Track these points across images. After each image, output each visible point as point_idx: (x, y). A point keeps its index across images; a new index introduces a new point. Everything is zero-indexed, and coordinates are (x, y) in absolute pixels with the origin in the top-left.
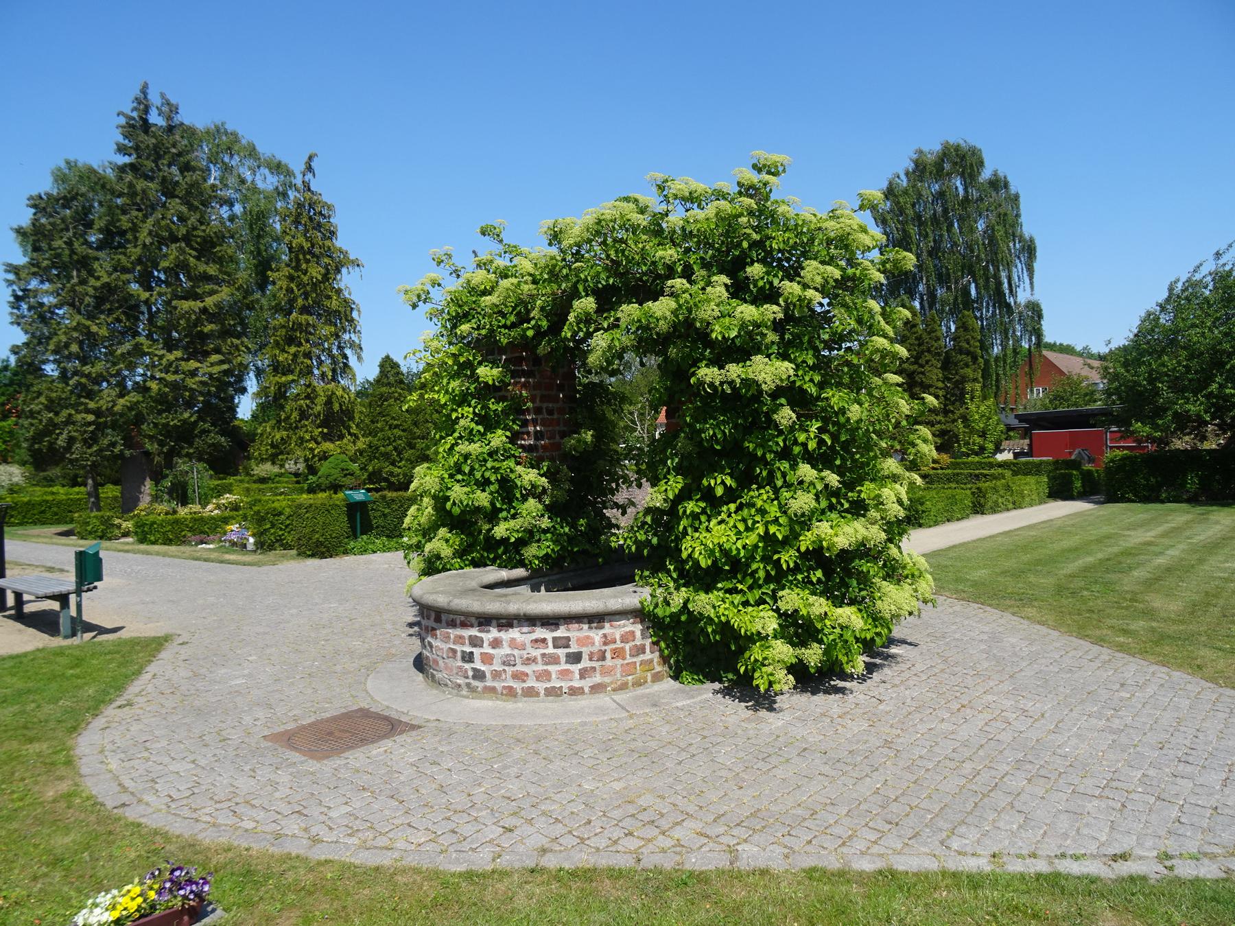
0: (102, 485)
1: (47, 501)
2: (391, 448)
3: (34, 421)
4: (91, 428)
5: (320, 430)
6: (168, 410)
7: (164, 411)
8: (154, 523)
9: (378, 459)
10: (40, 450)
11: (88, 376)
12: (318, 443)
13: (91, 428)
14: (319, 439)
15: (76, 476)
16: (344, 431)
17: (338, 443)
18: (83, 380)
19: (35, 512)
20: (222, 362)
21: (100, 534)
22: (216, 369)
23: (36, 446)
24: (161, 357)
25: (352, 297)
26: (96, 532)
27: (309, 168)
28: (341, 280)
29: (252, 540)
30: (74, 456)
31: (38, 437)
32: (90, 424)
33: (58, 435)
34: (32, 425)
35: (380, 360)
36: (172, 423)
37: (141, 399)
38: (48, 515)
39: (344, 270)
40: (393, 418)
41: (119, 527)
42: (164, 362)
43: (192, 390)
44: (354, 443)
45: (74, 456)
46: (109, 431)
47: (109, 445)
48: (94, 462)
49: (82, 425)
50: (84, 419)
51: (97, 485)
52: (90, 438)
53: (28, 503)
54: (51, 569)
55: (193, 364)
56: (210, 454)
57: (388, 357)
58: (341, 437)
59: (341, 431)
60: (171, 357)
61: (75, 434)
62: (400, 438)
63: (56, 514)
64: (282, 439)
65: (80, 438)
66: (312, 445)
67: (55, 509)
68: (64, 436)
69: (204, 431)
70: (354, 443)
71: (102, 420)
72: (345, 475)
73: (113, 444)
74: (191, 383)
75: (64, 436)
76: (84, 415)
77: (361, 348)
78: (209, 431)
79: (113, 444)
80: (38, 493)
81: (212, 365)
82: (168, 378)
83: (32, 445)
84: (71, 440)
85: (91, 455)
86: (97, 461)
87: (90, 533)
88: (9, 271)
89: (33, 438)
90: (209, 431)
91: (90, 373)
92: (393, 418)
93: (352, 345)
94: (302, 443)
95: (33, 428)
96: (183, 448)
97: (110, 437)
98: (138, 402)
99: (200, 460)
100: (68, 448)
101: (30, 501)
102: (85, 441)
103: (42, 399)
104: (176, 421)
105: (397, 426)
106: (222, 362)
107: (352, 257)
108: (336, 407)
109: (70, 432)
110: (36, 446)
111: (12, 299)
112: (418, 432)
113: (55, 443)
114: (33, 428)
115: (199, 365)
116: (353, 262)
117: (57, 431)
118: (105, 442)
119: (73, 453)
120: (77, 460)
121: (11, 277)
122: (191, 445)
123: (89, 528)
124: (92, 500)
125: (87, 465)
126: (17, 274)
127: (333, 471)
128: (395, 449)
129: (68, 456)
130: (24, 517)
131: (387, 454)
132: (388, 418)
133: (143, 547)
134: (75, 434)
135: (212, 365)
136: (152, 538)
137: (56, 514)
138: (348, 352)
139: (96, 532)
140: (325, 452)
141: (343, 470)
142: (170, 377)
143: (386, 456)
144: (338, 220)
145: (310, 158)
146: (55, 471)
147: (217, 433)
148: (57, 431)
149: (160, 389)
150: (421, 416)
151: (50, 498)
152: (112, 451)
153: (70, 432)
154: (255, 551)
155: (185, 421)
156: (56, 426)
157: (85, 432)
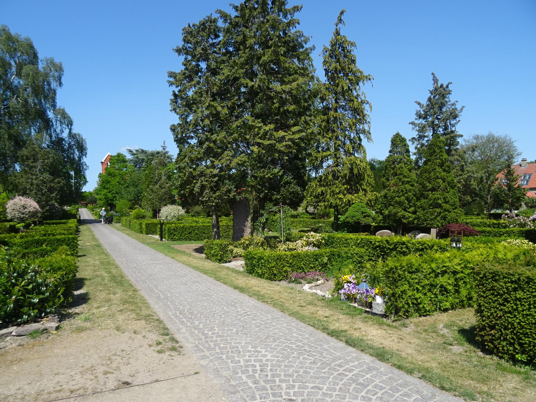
0: (220, 216)
1: (192, 227)
2: (403, 198)
3: (181, 174)
4: (216, 179)
5: (346, 186)
6: (264, 167)
7: (262, 168)
8: (261, 258)
9: (393, 206)
10: (184, 194)
11: (215, 142)
12: (345, 195)
13: (216, 179)
14: (345, 192)
15: (209, 212)
16: (359, 187)
17: (355, 195)
18: (212, 145)
19: (186, 233)
20: (300, 131)
21: (219, 258)
22: (297, 136)
23: (182, 192)
24: (260, 128)
25: (366, 99)
26: (217, 255)
27: (340, 20)
28: (359, 89)
29: (379, 300)
30: (204, 199)
31: (182, 186)
32: (215, 176)
33: (195, 184)
34: (180, 177)
35: (392, 136)
36: (267, 176)
37: (247, 160)
38: (193, 235)
39: (361, 84)
40: (405, 176)
41: (232, 251)
42: (262, 131)
43: (280, 152)
44: (365, 195)
45: (204, 199)
46: (227, 181)
47: (227, 192)
48: (217, 203)
49: (210, 177)
50: (211, 172)
51: (218, 217)
52: (215, 186)
53: (183, 227)
54: (157, 381)
55: (281, 133)
56: (290, 199)
57: (397, 135)
58: (357, 192)
59: (357, 187)
60: (267, 128)
61: (206, 183)
62: (410, 191)
63: (197, 234)
64: (322, 192)
65: (209, 186)
66: (341, 196)
67: (196, 231)
68: (199, 184)
69: (288, 183)
70: (365, 195)
71: (223, 173)
72: (365, 217)
73: (229, 191)
74: (280, 146)
75: (199, 184)
76: (212, 170)
77: (370, 133)
78: (290, 183)
79: (229, 191)
80: (189, 221)
81: (294, 133)
82: (265, 143)
83: (180, 192)
84: (203, 187)
85: (215, 198)
86: (219, 202)
87: (213, 256)
88: (171, 77)
89: (181, 186)
90: (290, 183)
91: (216, 140)
92: (405, 176)
93: (364, 131)
94: (334, 195)
95: (180, 179)
96: (273, 195)
97: (228, 185)
98: (245, 162)
99: (284, 203)
100: (201, 193)
101: (184, 226)
102: (212, 188)
103: (186, 159)
104: (269, 175)
105: (408, 182)
106: (300, 131)
107: (365, 74)
108: (355, 171)
109: (202, 181)
110: (182, 192)
111: (173, 97)
112: (430, 186)
113: (193, 190)
114: (180, 179)
115: (285, 134)
116: (366, 77)
117: (195, 181)
118: (225, 189)
119: (204, 197)
120: (206, 201)
121: (172, 79)
122: (278, 192)
123: (212, 252)
124: (215, 230)
125: (212, 206)
126: (175, 78)
127: (356, 214)
128: (407, 199)
129: (200, 199)
130: (181, 235)
131: (400, 202)
132: (401, 177)
133: (254, 282)
134: (206, 183)
135: (294, 133)
136: (260, 271)
137: (197, 234)
138: (362, 136)
139: (217, 255)
140: (349, 201)
141: (362, 213)
142: (266, 142)
143: (400, 204)
144: (356, 53)
145: (342, 13)
146: (198, 208)
147: (295, 184)
148: (195, 181)
149: (259, 151)
150: (432, 174)
151: (194, 225)
152: (229, 196)
153: (202, 181)
154: (385, 316)
155: (275, 175)
156: (194, 177)
157: (212, 181)
